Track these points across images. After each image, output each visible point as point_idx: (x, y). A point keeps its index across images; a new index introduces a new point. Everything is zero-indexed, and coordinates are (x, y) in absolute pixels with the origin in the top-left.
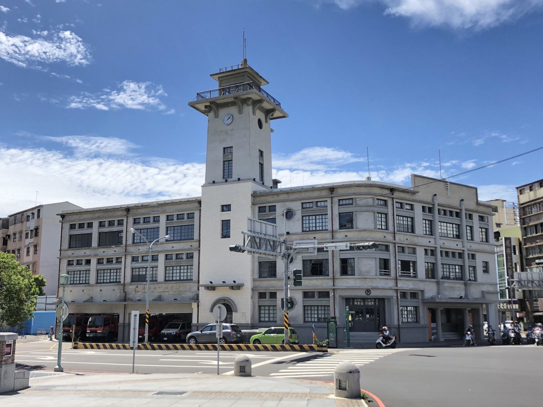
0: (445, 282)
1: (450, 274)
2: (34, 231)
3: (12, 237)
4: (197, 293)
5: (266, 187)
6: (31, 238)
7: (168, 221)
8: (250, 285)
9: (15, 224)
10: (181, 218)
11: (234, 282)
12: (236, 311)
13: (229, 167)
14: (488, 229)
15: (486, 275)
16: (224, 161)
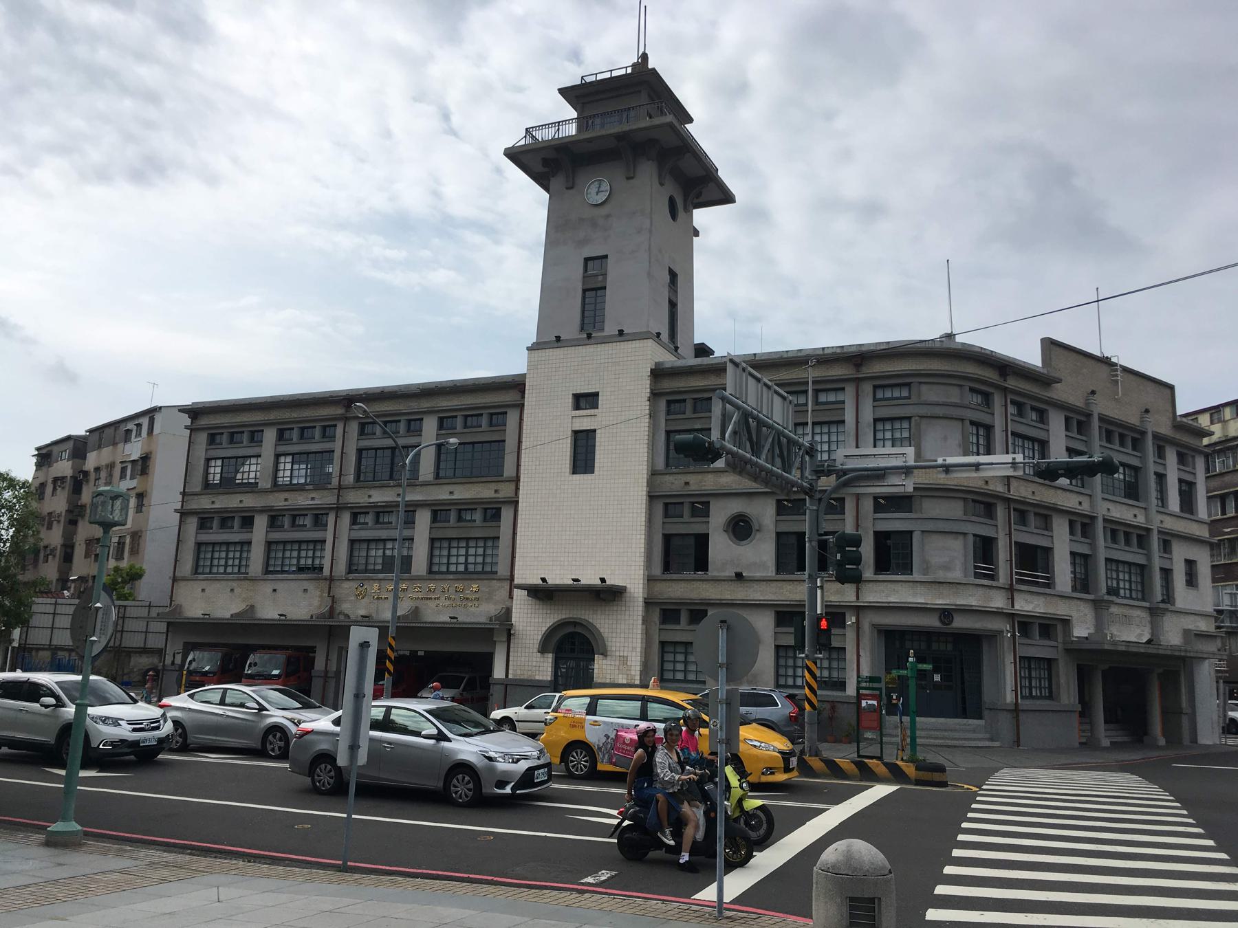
0: (1112, 602)
1: (1118, 584)
2: (140, 463)
3: (92, 476)
4: (508, 604)
5: (679, 357)
6: (132, 478)
7: (443, 432)
8: (641, 590)
9: (99, 447)
10: (475, 424)
11: (603, 580)
12: (604, 654)
13: (596, 304)
14: (1195, 483)
15: (1192, 592)
16: (584, 291)
